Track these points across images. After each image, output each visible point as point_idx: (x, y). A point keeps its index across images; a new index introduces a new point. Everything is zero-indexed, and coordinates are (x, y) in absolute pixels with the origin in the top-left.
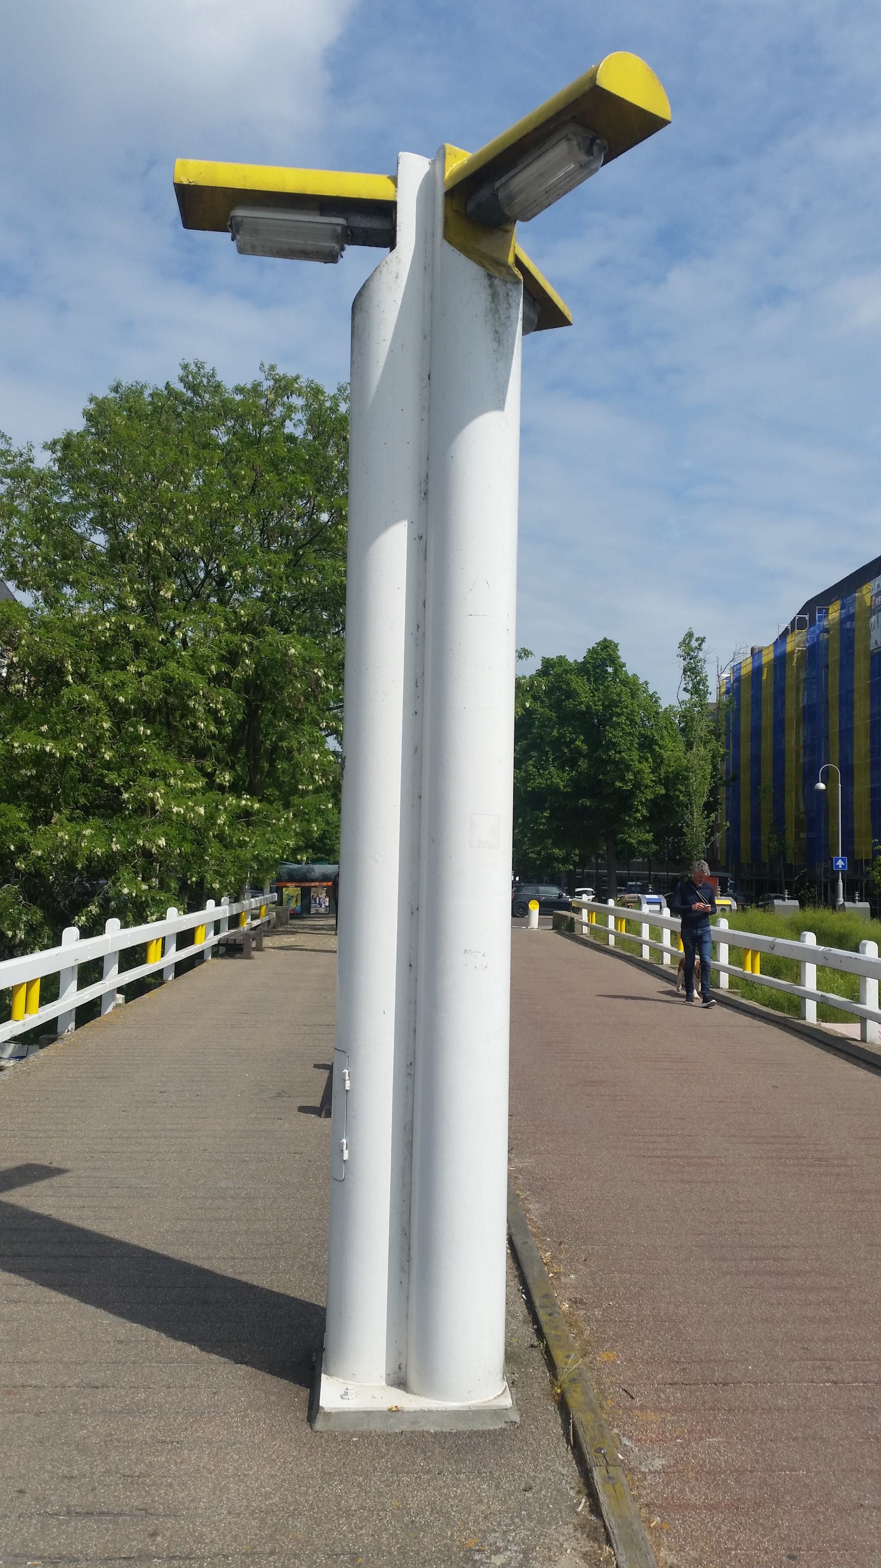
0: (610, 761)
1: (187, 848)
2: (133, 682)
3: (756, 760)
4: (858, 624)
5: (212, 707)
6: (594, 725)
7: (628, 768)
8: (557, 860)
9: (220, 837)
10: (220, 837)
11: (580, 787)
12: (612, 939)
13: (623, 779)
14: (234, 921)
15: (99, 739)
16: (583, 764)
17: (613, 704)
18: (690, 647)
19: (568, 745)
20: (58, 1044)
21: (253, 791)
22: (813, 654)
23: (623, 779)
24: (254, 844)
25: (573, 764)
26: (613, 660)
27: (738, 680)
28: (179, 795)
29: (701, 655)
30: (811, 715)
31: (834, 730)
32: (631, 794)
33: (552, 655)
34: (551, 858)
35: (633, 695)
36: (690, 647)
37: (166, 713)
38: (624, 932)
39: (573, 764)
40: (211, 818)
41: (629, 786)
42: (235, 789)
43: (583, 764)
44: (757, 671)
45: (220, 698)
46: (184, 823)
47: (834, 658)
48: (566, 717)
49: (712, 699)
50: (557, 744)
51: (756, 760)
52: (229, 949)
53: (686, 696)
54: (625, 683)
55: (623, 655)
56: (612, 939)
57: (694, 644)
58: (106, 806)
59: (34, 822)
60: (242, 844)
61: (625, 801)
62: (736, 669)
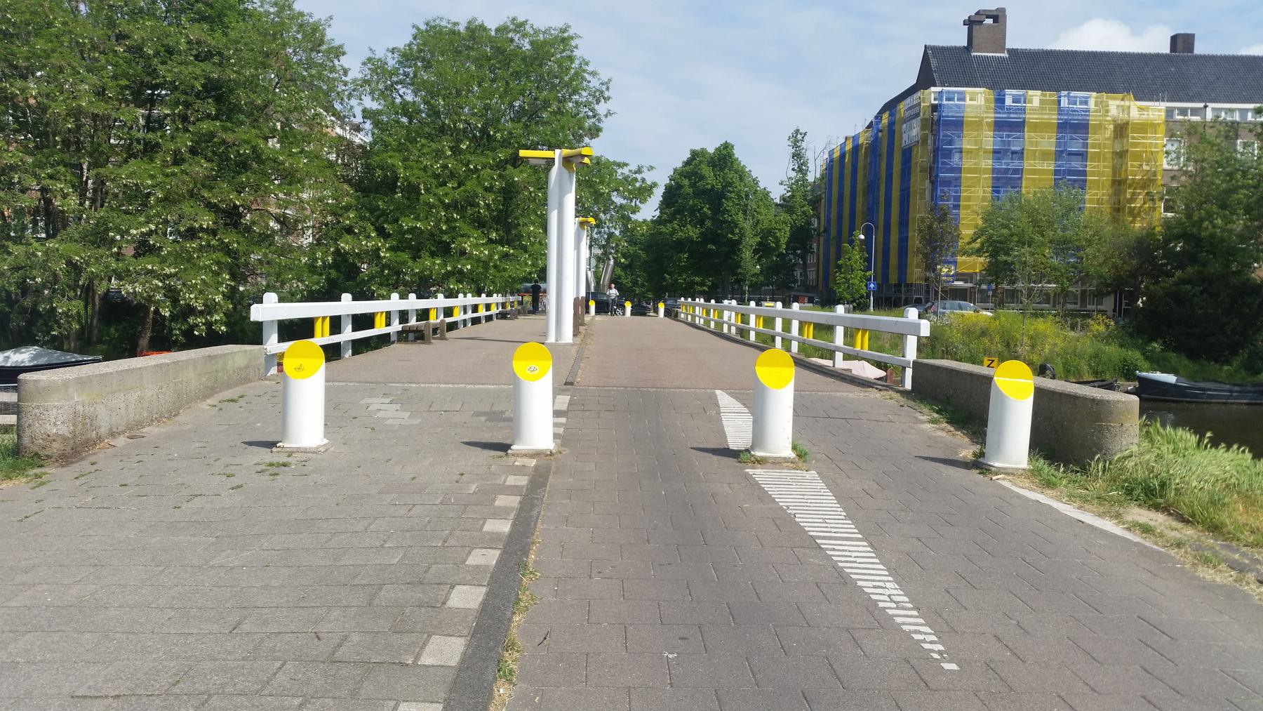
0: (726, 222)
1: (481, 270)
2: (450, 192)
3: (840, 217)
4: (896, 127)
5: (486, 202)
6: (716, 198)
7: (736, 226)
8: (697, 283)
9: (495, 266)
10: (495, 266)
11: (708, 237)
12: (752, 334)
13: (733, 233)
14: (504, 305)
15: (440, 221)
16: (708, 223)
17: (730, 184)
18: (797, 139)
19: (699, 210)
20: (595, 51)
21: (509, 243)
22: (874, 146)
23: (733, 233)
24: (511, 269)
25: (702, 222)
26: (730, 155)
27: (832, 161)
28: (474, 244)
29: (804, 145)
30: (871, 188)
31: (882, 199)
32: (738, 242)
33: (698, 148)
34: (693, 283)
35: (741, 179)
36: (797, 139)
37: (463, 206)
38: (811, 338)
39: (702, 222)
40: (491, 256)
41: (737, 238)
42: (501, 242)
43: (708, 223)
44: (842, 156)
45: (490, 198)
46: (478, 260)
47: (884, 149)
48: (701, 193)
49: (811, 178)
50: (693, 210)
51: (840, 217)
52: (502, 316)
53: (793, 174)
54: (736, 172)
55: (737, 153)
56: (752, 334)
57: (799, 137)
58: (443, 250)
59: (414, 259)
60: (505, 270)
61: (735, 246)
62: (831, 153)
